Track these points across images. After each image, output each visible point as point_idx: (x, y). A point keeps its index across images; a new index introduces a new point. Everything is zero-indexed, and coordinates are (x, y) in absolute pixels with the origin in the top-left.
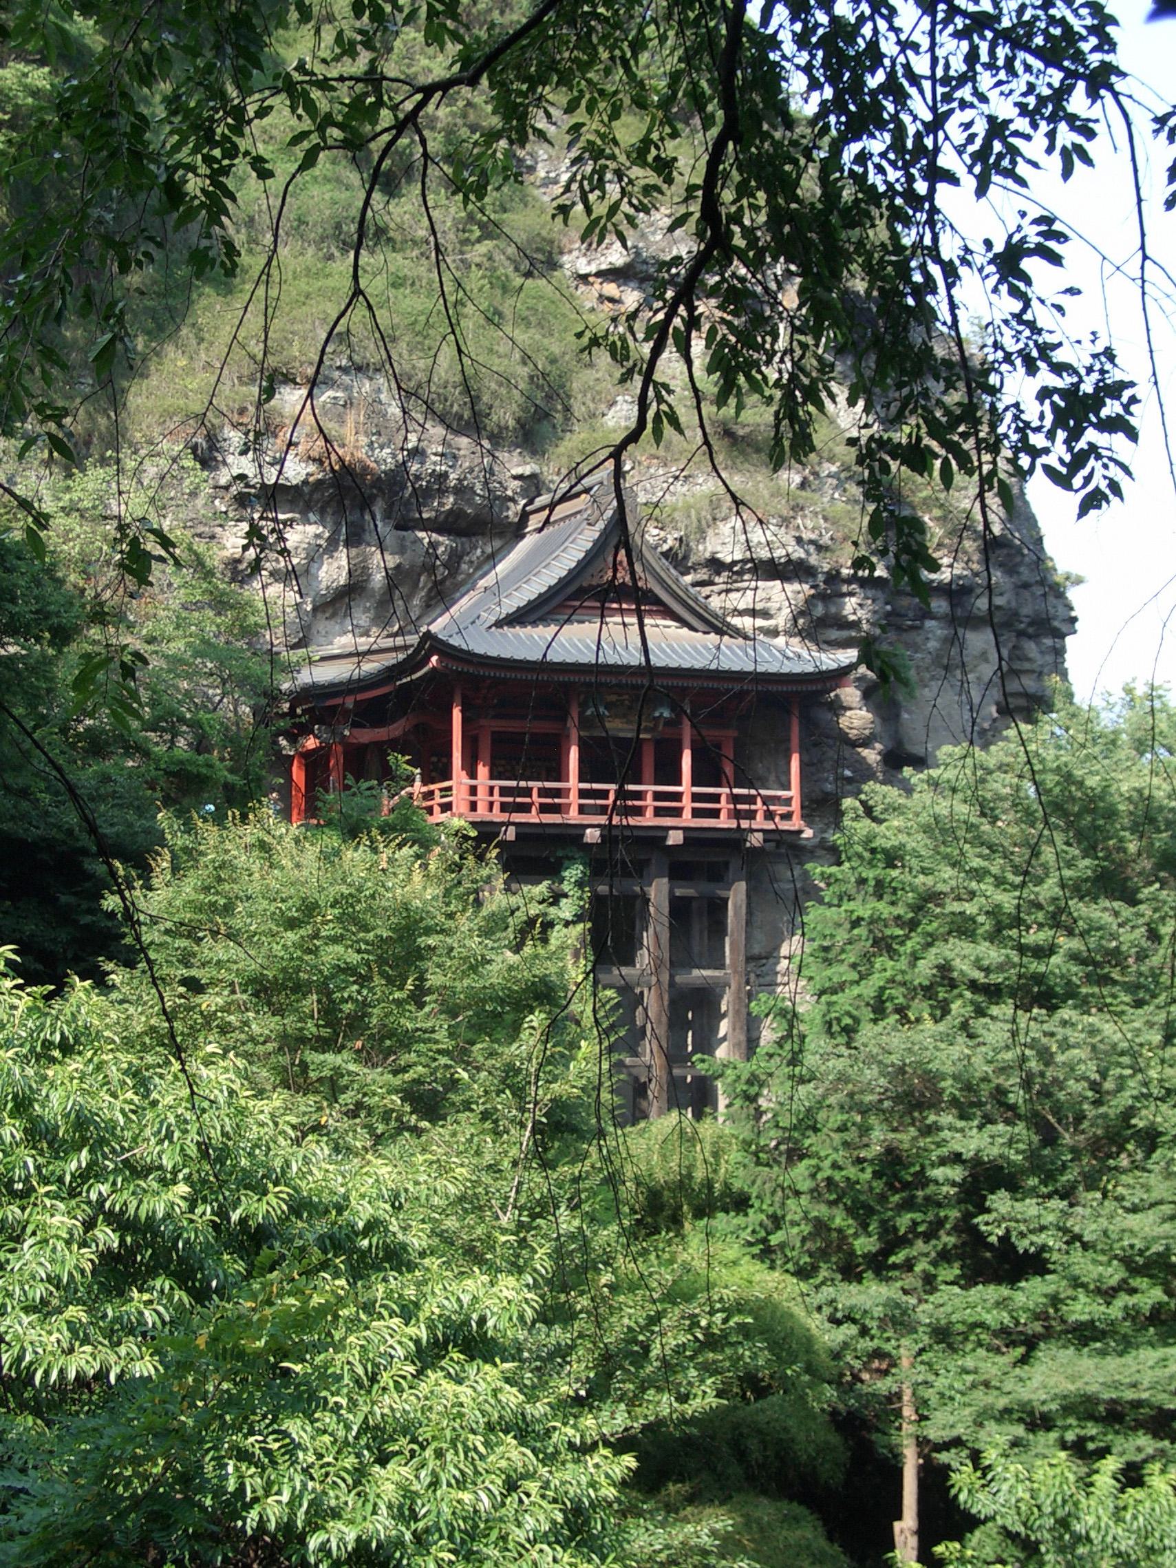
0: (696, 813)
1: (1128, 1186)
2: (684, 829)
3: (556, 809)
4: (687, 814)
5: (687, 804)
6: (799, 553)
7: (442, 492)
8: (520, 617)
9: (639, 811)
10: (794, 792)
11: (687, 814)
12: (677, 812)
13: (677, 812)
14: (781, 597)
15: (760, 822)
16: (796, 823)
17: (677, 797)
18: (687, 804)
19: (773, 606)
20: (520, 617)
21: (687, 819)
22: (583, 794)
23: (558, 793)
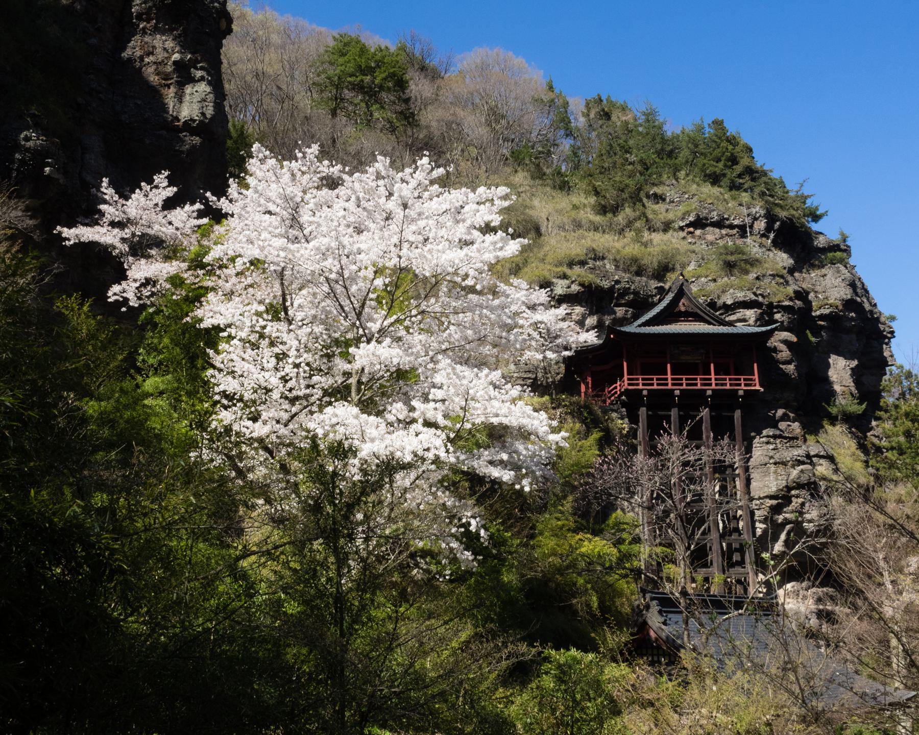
0: (716, 385)
1: (760, 592)
2: (712, 390)
3: (722, 385)
4: (714, 385)
5: (713, 381)
6: (754, 298)
7: (628, 294)
8: (640, 326)
9: (696, 385)
10: (756, 376)
11: (714, 385)
12: (740, 385)
13: (740, 385)
14: (751, 314)
15: (743, 387)
16: (758, 387)
17: (710, 379)
18: (713, 381)
19: (747, 317)
20: (640, 326)
21: (713, 387)
22: (673, 379)
23: (751, 380)
